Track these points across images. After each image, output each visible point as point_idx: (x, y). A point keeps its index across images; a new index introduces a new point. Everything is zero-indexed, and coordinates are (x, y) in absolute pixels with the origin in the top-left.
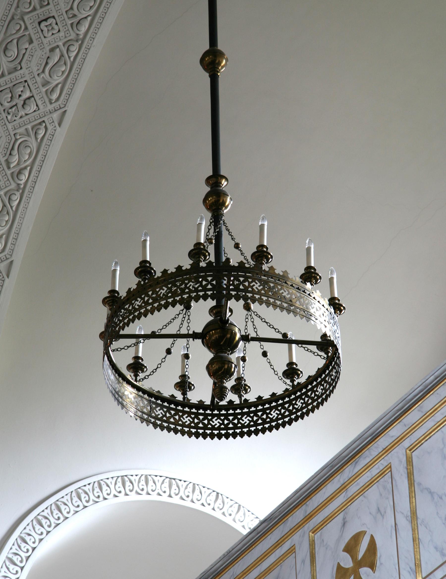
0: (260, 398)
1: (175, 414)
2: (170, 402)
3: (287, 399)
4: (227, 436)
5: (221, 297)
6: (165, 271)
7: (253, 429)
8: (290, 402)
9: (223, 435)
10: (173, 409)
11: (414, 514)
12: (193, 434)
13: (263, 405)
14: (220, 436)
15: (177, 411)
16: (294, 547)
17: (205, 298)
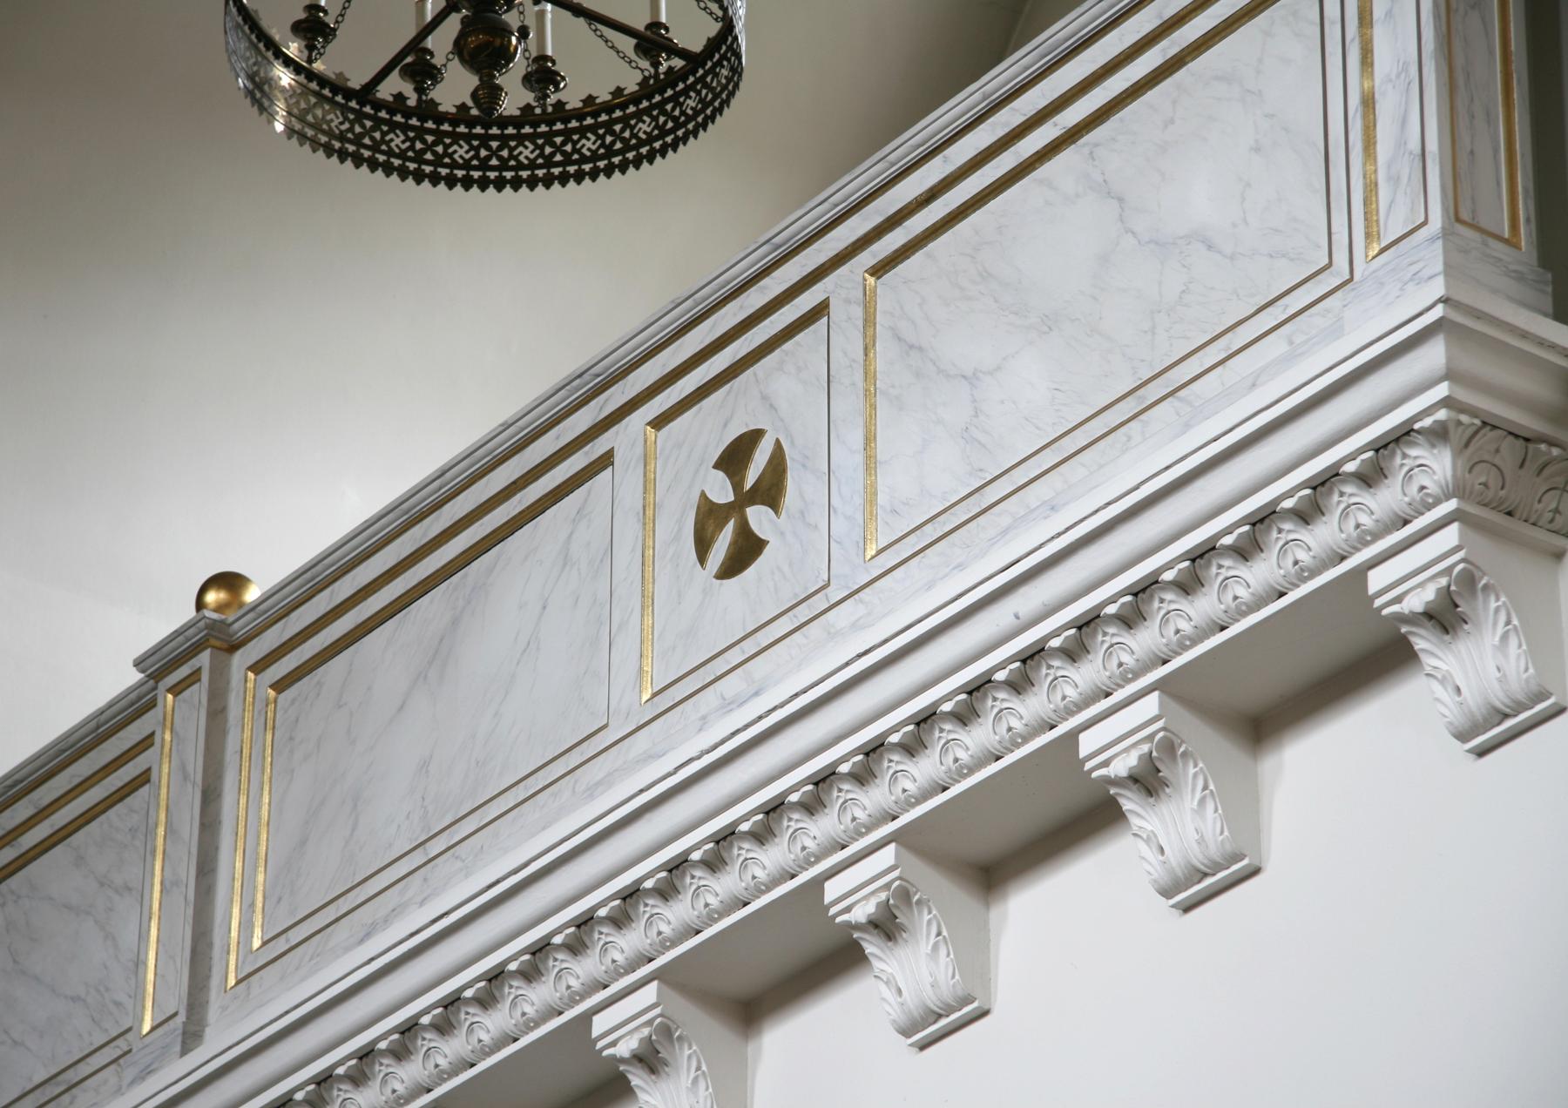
1: (373, 129)
3: (618, 113)
4: (483, 184)
7: (540, 173)
8: (624, 120)
9: (492, 182)
10: (368, 117)
11: (869, 375)
12: (426, 176)
13: (566, 121)
14: (467, 183)
15: (440, 135)
16: (122, 1044)
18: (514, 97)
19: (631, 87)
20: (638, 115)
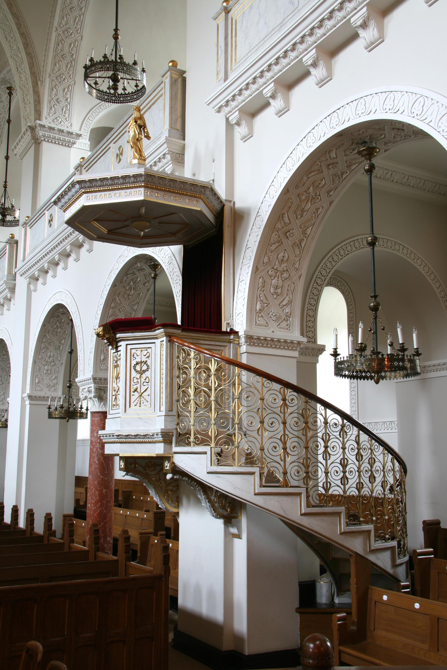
0: (129, 93)
2: (105, 93)
5: (116, 70)
6: (97, 61)
17: (111, 70)
18: (120, 91)
19: (134, 91)
20: (134, 95)
